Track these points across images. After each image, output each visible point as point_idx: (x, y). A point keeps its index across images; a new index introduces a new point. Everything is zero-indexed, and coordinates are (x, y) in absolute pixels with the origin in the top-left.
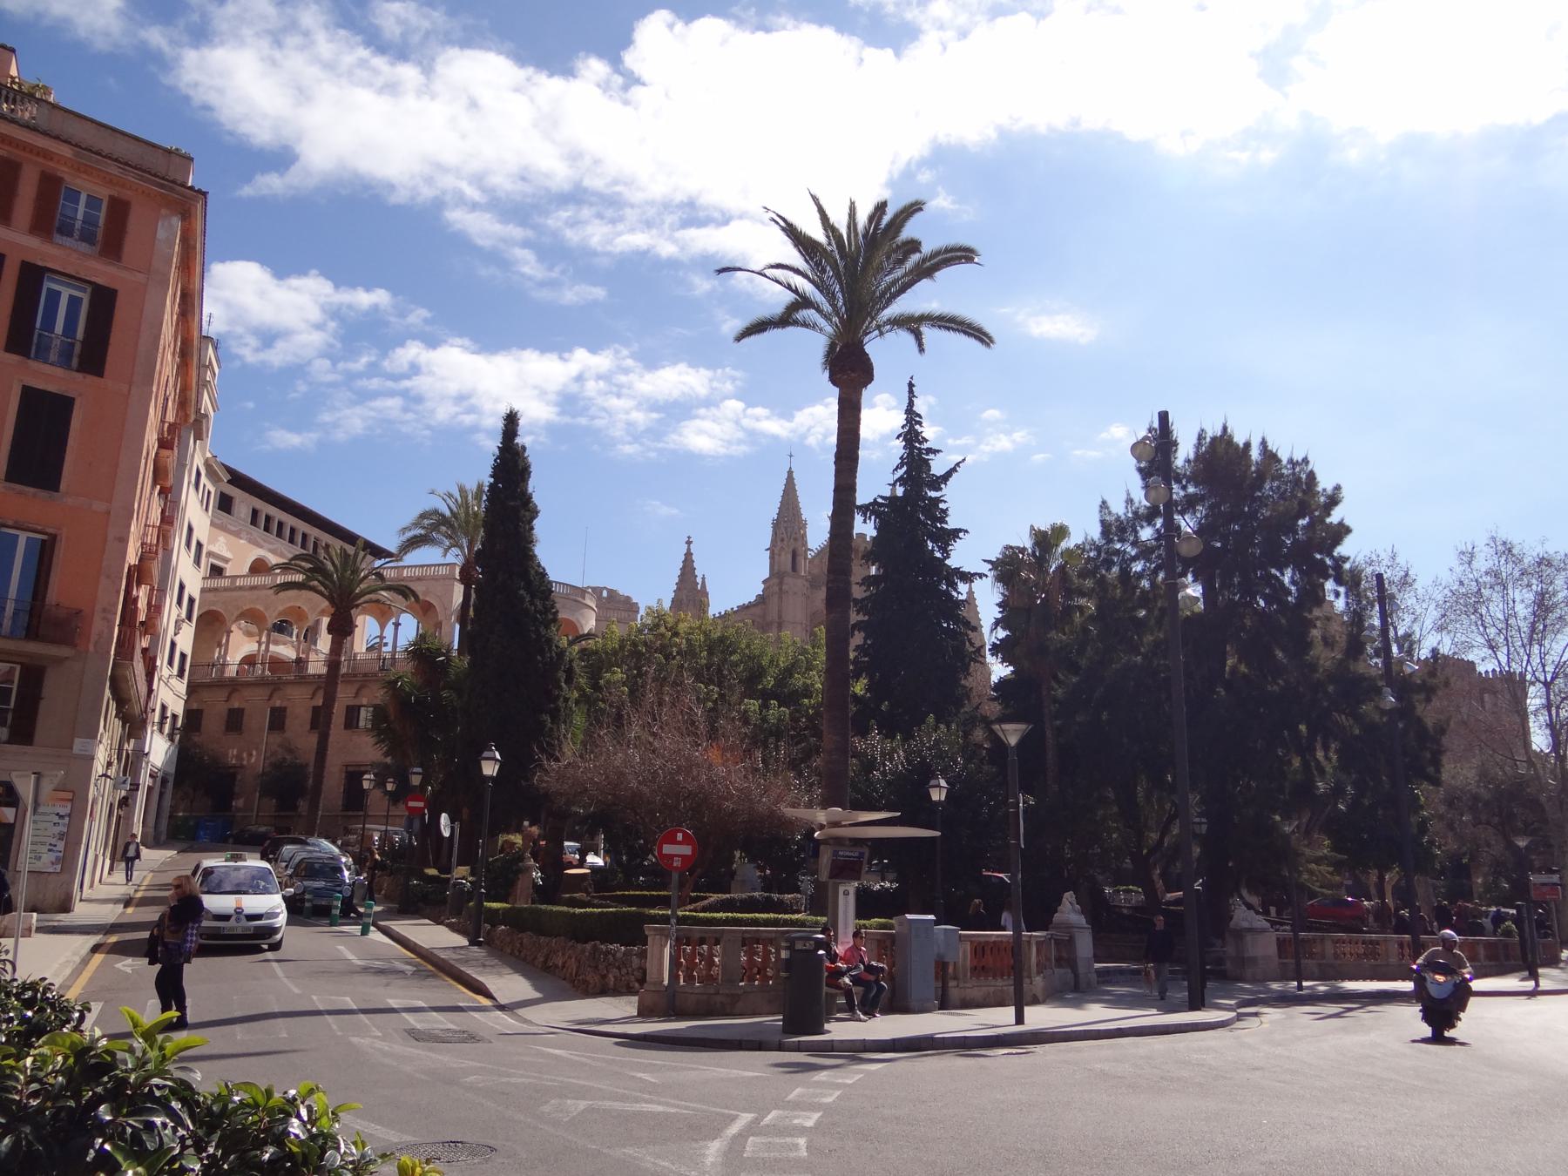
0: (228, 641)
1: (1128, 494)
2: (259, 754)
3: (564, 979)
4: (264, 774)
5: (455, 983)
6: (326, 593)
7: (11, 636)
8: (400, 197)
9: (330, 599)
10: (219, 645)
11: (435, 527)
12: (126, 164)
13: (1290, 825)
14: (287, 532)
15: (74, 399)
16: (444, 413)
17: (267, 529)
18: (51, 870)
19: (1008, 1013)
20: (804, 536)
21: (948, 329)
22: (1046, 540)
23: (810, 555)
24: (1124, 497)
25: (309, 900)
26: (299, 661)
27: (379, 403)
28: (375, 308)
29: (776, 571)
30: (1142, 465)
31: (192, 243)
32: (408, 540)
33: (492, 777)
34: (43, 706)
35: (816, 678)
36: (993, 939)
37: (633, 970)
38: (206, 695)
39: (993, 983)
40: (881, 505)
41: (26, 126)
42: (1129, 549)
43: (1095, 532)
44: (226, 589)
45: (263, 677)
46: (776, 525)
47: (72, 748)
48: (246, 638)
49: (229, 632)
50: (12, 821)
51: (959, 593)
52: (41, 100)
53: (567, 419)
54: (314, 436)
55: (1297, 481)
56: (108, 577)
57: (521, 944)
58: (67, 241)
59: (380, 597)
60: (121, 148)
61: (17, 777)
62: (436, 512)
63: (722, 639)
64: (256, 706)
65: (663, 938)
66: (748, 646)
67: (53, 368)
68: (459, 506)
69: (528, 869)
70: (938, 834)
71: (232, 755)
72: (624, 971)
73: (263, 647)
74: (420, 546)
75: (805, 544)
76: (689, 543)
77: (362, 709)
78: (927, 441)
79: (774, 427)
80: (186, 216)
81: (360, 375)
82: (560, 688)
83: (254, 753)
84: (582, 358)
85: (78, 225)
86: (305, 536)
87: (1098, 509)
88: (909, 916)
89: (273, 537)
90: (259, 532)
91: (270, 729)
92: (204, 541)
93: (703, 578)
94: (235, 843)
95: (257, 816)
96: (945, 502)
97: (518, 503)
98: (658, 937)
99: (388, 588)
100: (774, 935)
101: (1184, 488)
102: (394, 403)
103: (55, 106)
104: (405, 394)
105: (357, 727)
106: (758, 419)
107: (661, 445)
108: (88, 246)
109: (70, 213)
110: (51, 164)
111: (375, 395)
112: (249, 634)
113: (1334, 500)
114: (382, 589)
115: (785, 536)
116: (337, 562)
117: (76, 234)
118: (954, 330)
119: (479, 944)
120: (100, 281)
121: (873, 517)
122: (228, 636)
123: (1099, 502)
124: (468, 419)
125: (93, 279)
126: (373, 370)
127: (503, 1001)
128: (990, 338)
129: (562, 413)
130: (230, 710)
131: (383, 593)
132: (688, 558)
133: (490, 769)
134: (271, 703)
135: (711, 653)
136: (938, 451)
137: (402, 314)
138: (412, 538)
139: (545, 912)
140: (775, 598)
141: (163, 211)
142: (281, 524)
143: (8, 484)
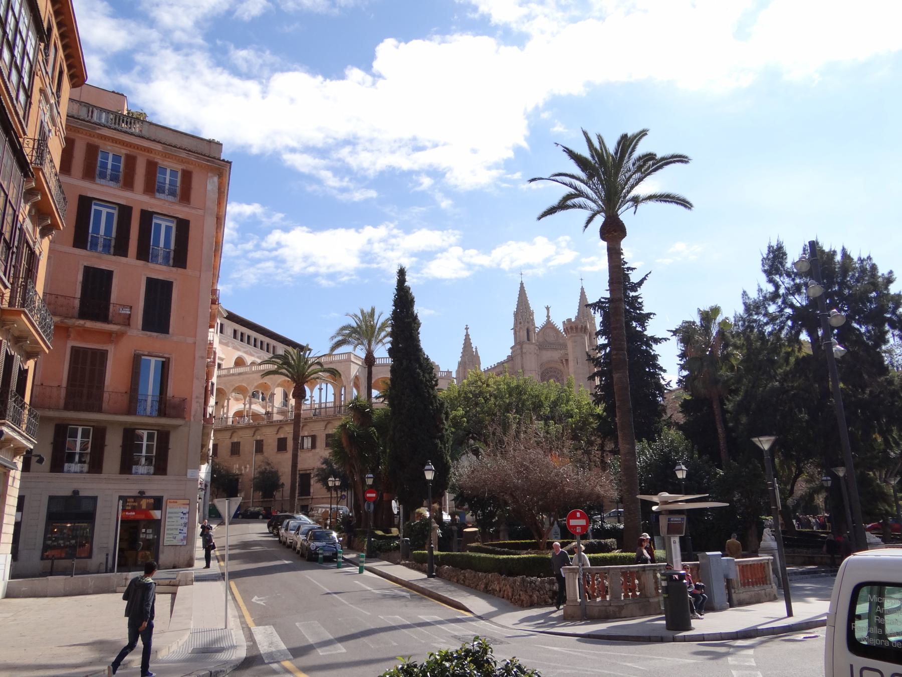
1: (759, 286)
2: (251, 467)
3: (503, 598)
4: (254, 478)
5: (439, 603)
8: (255, 150)
10: (223, 407)
11: (350, 335)
13: (895, 480)
14: (252, 341)
16: (297, 268)
17: (249, 343)
18: (180, 544)
19: (779, 607)
20: (533, 320)
21: (666, 201)
22: (708, 316)
23: (537, 330)
24: (757, 288)
25: (321, 554)
26: (267, 413)
27: (261, 265)
28: (254, 215)
29: (518, 341)
30: (766, 268)
31: (222, 190)
33: (430, 481)
34: (170, 453)
35: (574, 406)
36: (750, 563)
37: (547, 592)
39: (753, 589)
40: (603, 303)
42: (762, 319)
43: (741, 310)
44: (225, 376)
46: (516, 315)
47: (186, 475)
48: (236, 402)
49: (228, 400)
50: (160, 518)
51: (653, 350)
52: (143, 121)
53: (364, 266)
54: (230, 286)
55: (863, 270)
56: (198, 379)
57: (465, 577)
58: (162, 196)
60: (186, 143)
63: (518, 387)
64: (247, 441)
65: (574, 574)
66: (532, 389)
69: (434, 529)
70: (728, 504)
71: (235, 468)
72: (542, 592)
73: (247, 406)
74: (341, 346)
75: (533, 324)
76: (467, 329)
78: (627, 263)
79: (483, 260)
81: (250, 251)
82: (443, 424)
83: (248, 466)
84: (369, 231)
85: (167, 186)
87: (741, 296)
88: (708, 553)
89: (245, 344)
90: (238, 342)
91: (256, 452)
93: (476, 348)
94: (242, 518)
95: (253, 502)
96: (641, 298)
97: (411, 320)
98: (571, 574)
99: (325, 371)
100: (637, 569)
101: (793, 280)
102: (270, 264)
103: (151, 124)
104: (275, 259)
105: (303, 449)
106: (471, 257)
107: (419, 275)
108: (173, 198)
109: (162, 181)
110: (151, 155)
111: (259, 261)
112: (237, 400)
113: (889, 280)
114: (321, 371)
115: (521, 320)
116: (295, 358)
117: (167, 192)
118: (668, 201)
119: (433, 577)
120: (180, 216)
121: (599, 310)
122: (228, 402)
123: (742, 292)
124: (312, 269)
126: (258, 247)
127: (479, 614)
128: (690, 204)
129: (363, 262)
130: (232, 443)
132: (467, 338)
133: (429, 476)
134: (255, 438)
135: (511, 395)
136: (634, 269)
137: (269, 216)
138: (338, 342)
139: (475, 557)
140: (519, 357)
141: (209, 174)
142: (249, 337)
143: (144, 332)
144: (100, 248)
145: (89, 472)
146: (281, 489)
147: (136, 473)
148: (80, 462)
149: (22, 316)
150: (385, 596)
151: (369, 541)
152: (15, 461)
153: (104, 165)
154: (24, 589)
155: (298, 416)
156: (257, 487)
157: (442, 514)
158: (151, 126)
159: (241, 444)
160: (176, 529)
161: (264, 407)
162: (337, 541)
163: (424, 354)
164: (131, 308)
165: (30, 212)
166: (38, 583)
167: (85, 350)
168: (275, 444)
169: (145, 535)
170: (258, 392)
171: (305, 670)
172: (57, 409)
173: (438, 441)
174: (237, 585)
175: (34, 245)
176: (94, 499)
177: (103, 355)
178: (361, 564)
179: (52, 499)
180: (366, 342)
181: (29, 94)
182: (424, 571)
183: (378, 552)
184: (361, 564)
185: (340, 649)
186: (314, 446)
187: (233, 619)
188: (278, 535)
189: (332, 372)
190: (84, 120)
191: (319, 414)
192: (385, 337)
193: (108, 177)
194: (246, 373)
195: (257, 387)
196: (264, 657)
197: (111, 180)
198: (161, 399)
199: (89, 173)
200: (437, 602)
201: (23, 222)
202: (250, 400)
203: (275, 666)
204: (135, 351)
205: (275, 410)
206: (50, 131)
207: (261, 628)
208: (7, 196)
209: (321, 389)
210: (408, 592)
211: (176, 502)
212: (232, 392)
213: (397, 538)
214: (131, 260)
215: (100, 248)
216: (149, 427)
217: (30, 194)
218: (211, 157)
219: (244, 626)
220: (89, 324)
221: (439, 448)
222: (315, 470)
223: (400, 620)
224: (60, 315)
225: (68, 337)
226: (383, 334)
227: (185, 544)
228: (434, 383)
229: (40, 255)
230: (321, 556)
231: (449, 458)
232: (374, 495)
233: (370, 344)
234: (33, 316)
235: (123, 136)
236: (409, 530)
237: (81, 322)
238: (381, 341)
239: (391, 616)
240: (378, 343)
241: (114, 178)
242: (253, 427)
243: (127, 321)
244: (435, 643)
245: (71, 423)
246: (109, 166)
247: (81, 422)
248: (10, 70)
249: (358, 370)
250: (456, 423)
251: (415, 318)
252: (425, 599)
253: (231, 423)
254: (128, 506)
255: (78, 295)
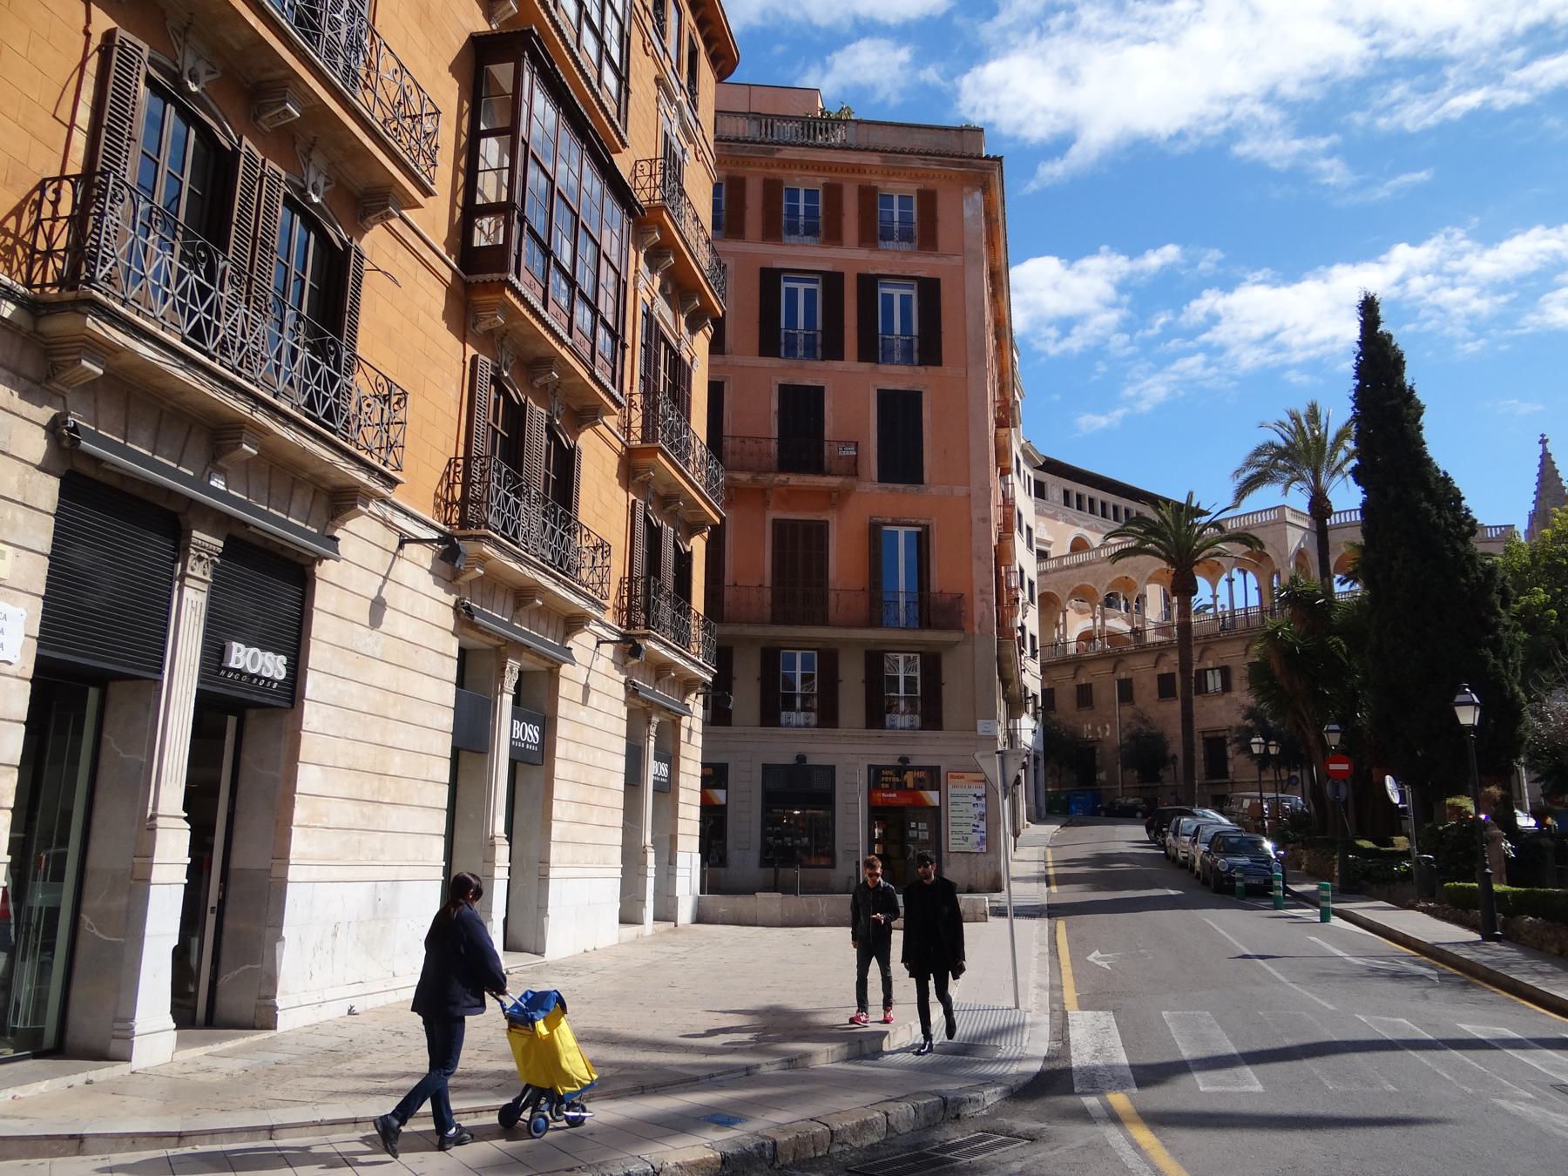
0: (1065, 619)
2: (1113, 727)
4: (1122, 746)
6: (1163, 554)
7: (906, 628)
9: (1169, 560)
10: (1057, 625)
12: (927, 154)
15: (921, 393)
17: (1080, 508)
18: (977, 850)
25: (1240, 880)
26: (1135, 631)
31: (994, 216)
32: (1245, 482)
33: (1471, 727)
38: (1055, 674)
41: (844, 148)
44: (1055, 571)
45: (1104, 652)
47: (976, 730)
49: (1065, 611)
56: (979, 558)
58: (890, 245)
59: (1219, 550)
60: (920, 141)
61: (982, 757)
62: (1272, 445)
64: (1103, 681)
67: (897, 367)
68: (1294, 434)
73: (1099, 622)
74: (1257, 487)
76: (1543, 442)
77: (1209, 673)
80: (986, 188)
82: (1498, 615)
83: (1108, 726)
85: (896, 226)
86: (1115, 508)
89: (1086, 514)
92: (1032, 526)
94: (1106, 816)
103: (858, 122)
105: (1207, 692)
112: (1081, 612)
114: (1223, 540)
119: (1497, 939)
122: (1065, 616)
125: (917, 274)
131: (1221, 545)
132: (1546, 461)
133: (1468, 717)
138: (1249, 479)
141: (966, 190)
142: (1091, 501)
144: (800, 353)
145: (818, 726)
146: (1172, 766)
147: (892, 727)
148: (804, 709)
149: (659, 456)
150: (1374, 972)
151: (1344, 860)
152: (687, 701)
153: (793, 211)
154: (722, 910)
155: (1185, 627)
156: (1128, 763)
157: (1515, 815)
158: (860, 126)
159: (1094, 687)
160: (967, 824)
161: (1130, 622)
162: (1274, 857)
163: (1438, 471)
164: (857, 444)
165: (662, 289)
166: (741, 903)
167: (794, 524)
168: (1154, 686)
169: (916, 832)
170: (1115, 595)
171: (1158, 1120)
172: (760, 622)
173: (1488, 652)
174: (1068, 928)
175: (679, 346)
176: (831, 769)
177: (822, 528)
178: (1324, 904)
179: (767, 769)
180: (1308, 474)
181: (624, 75)
182: (1472, 927)
183: (1365, 883)
184: (1324, 904)
185: (1250, 1084)
186: (1227, 687)
187: (1036, 991)
188: (1163, 846)
189: (1245, 539)
190: (754, 142)
191: (1230, 627)
192: (1347, 459)
193: (802, 230)
194: (1090, 563)
195: (1112, 585)
196: (1075, 1079)
197: (807, 234)
198: (921, 597)
199: (772, 232)
200: (1505, 994)
201: (652, 304)
202: (1102, 609)
203: (1091, 1102)
204: (871, 518)
205: (1150, 626)
206: (684, 151)
207: (1089, 1014)
208: (598, 246)
209: (1230, 581)
210: (1432, 967)
211: (962, 777)
212: (1069, 598)
213: (1406, 855)
214: (850, 363)
215: (800, 353)
216: (910, 648)
217: (657, 257)
218: (964, 157)
219: (1056, 1006)
220: (794, 480)
221: (1490, 666)
222: (1234, 731)
223: (1408, 1028)
224: (750, 470)
225: (766, 503)
226: (1342, 454)
227: (985, 850)
228: (1466, 529)
229: (692, 363)
230: (1238, 884)
231: (1517, 688)
232: (1345, 767)
233: (1316, 478)
234: (687, 464)
235: (818, 154)
236: (1428, 840)
237: (783, 477)
238: (1339, 468)
239: (1386, 1019)
240: (1333, 474)
241: (811, 230)
242: (1110, 657)
243: (852, 468)
244: (1501, 1097)
245: (783, 644)
246: (802, 212)
247: (800, 644)
248: (579, 28)
249: (1303, 538)
250: (1531, 620)
251: (1408, 396)
252: (1475, 986)
253: (1074, 652)
254: (884, 782)
255: (775, 434)
